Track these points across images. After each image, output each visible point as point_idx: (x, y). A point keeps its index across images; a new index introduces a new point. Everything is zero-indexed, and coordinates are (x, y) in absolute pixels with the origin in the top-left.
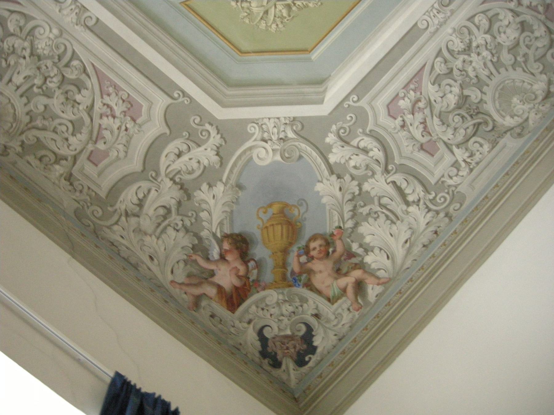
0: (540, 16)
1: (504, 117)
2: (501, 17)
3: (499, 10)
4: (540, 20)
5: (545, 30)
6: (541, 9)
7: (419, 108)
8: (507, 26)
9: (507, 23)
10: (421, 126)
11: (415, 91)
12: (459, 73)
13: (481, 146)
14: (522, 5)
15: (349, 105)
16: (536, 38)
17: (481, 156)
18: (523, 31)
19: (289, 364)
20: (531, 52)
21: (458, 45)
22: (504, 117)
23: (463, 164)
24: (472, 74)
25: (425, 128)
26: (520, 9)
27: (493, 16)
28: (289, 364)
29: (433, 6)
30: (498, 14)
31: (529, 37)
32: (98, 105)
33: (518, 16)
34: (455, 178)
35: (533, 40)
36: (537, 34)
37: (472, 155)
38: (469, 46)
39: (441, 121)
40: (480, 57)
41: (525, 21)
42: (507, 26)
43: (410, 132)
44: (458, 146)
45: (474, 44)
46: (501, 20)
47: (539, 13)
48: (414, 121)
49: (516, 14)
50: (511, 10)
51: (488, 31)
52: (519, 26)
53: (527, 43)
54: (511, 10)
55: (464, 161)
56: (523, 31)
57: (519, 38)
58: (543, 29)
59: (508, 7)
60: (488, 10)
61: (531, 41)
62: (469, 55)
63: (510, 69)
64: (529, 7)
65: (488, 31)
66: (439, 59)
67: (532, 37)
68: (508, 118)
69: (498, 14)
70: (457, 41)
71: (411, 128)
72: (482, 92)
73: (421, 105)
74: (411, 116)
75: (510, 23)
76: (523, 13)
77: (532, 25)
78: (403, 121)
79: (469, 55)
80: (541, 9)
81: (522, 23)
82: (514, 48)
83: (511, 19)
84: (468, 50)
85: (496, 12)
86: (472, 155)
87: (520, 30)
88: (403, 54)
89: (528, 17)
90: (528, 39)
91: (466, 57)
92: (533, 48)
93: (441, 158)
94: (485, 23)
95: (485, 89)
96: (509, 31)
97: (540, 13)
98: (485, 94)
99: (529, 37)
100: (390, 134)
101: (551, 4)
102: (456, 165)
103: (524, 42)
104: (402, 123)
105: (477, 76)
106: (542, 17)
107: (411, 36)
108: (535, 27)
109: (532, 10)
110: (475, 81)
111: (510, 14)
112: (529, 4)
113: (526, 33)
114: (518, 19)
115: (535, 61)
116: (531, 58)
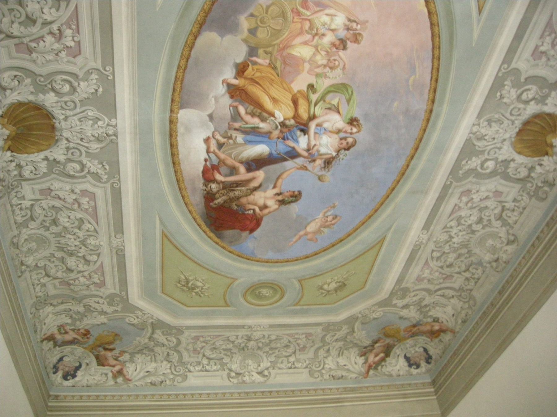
0: (28, 39)
1: (28, 235)
2: (53, 10)
3: (60, 13)
4: (24, 37)
5: (13, 34)
6: (33, 45)
7: (74, 204)
8: (42, 9)
9: (44, 11)
10: (63, 197)
11: (87, 209)
12: (74, 232)
13: (23, 216)
14: (48, 34)
15: (114, 177)
16: (13, 22)
17: (17, 214)
18: (27, 17)
19: (60, 374)
20: (52, 265)
21: (91, 241)
22: (28, 235)
23: (19, 202)
24: (68, 236)
25: (60, 199)
26: (46, 30)
27: (59, 6)
28: (60, 374)
29: (124, 246)
30: (58, 10)
31: (18, 18)
32: (55, 27)
33: (43, 24)
34: (15, 194)
35: (13, 19)
36: (16, 25)
37: (21, 209)
38: (84, 245)
39: (56, 207)
40: (74, 245)
41: (34, 26)
42: (42, 9)
43: (66, 191)
44: (32, 205)
45: (83, 248)
46: (50, 8)
47: (30, 41)
48: (70, 198)
49: (46, 23)
50: (51, 23)
51: (84, 257)
52: (34, 18)
53: (16, 12)
54: (51, 23)
55: (21, 204)
56: (27, 17)
57: (24, 9)
58: (16, 33)
59: (56, 22)
60: (67, 5)
61: (14, 16)
62: (80, 242)
63: (53, 252)
64: (42, 38)
65: (84, 257)
66: (92, 229)
67: (16, 20)
68: (26, 237)
69: (58, 10)
70: (93, 242)
71: (68, 193)
72: (53, 233)
73: (76, 206)
74: (74, 198)
75: (43, 13)
76: (41, 29)
77: (26, 28)
78: (76, 193)
79: (80, 242)
80: (33, 45)
81: (34, 22)
82: (62, 260)
83: (45, 17)
84: (83, 243)
85: (61, 9)
86: (21, 209)
87: (30, 16)
88: (100, 18)
89: (35, 30)
90: (18, 15)
91: (80, 240)
92: (6, 12)
93: (34, 193)
94: (89, 258)
95: (54, 235)
96: (37, 6)
97: (30, 41)
98: (51, 234)
99: (18, 18)
100: (75, 183)
101: (30, 55)
102: (23, 198)
103: (18, 11)
104: (75, 191)
105: (64, 237)
106: (26, 40)
107: (119, 227)
108: (22, 28)
109: (39, 38)
110: (63, 234)
111: (49, 19)
112: (45, 39)
113: (23, 18)
114: (40, 21)
115: (45, 265)
116: (48, 263)
